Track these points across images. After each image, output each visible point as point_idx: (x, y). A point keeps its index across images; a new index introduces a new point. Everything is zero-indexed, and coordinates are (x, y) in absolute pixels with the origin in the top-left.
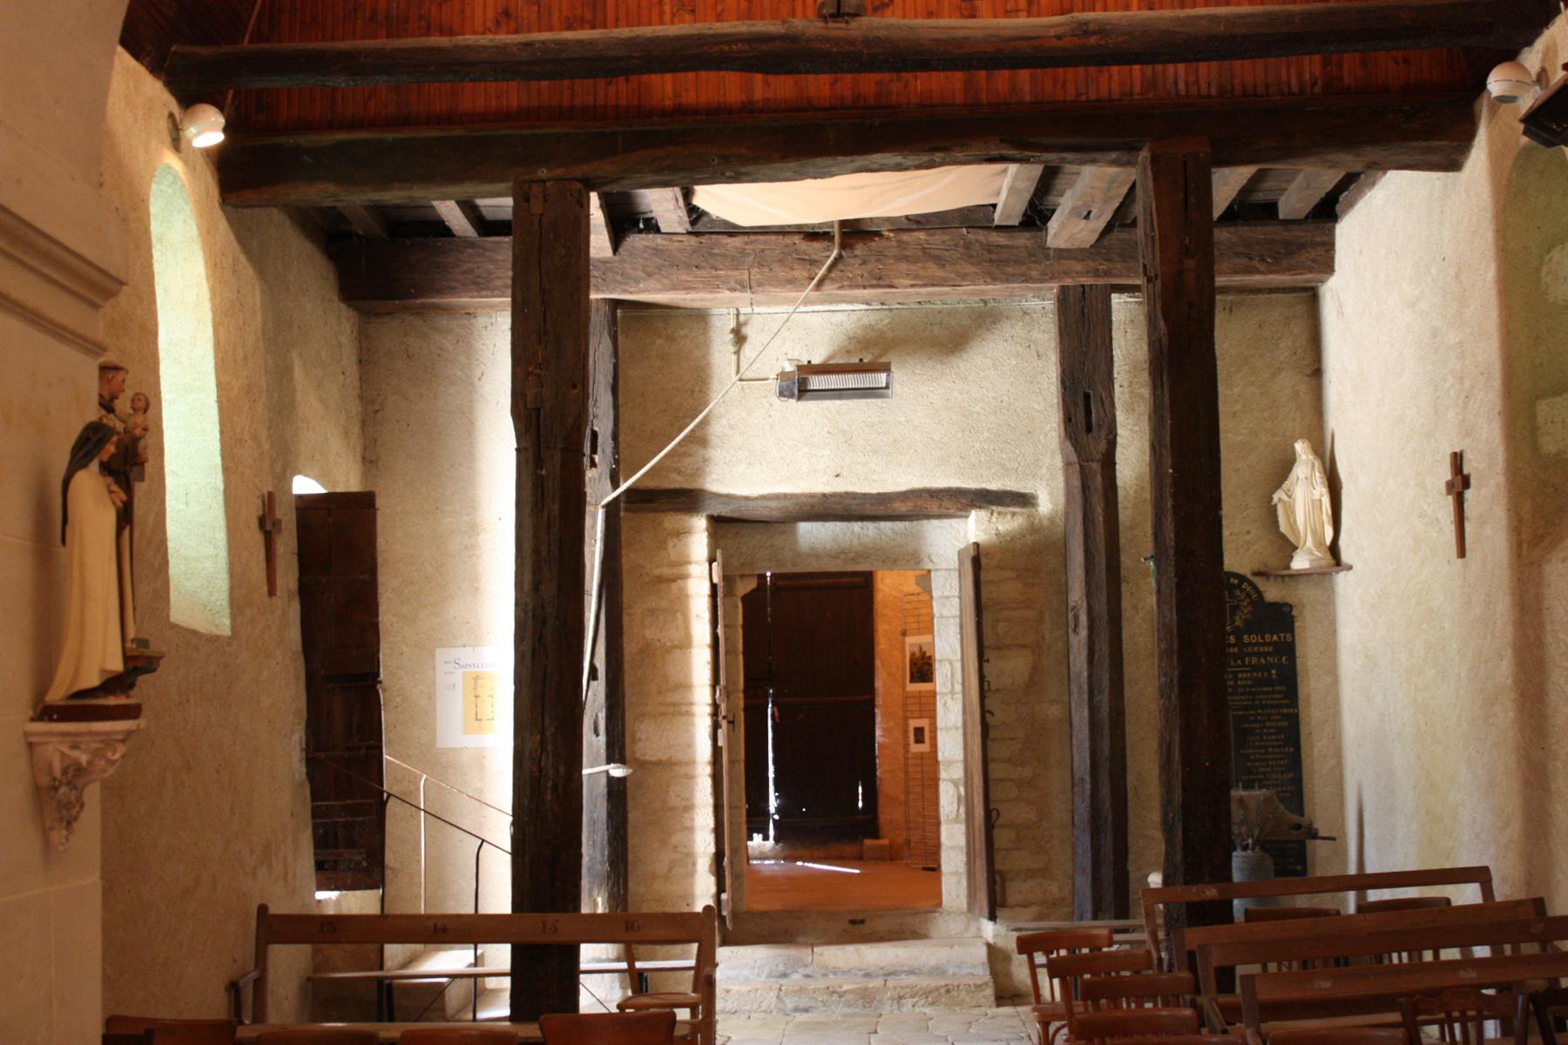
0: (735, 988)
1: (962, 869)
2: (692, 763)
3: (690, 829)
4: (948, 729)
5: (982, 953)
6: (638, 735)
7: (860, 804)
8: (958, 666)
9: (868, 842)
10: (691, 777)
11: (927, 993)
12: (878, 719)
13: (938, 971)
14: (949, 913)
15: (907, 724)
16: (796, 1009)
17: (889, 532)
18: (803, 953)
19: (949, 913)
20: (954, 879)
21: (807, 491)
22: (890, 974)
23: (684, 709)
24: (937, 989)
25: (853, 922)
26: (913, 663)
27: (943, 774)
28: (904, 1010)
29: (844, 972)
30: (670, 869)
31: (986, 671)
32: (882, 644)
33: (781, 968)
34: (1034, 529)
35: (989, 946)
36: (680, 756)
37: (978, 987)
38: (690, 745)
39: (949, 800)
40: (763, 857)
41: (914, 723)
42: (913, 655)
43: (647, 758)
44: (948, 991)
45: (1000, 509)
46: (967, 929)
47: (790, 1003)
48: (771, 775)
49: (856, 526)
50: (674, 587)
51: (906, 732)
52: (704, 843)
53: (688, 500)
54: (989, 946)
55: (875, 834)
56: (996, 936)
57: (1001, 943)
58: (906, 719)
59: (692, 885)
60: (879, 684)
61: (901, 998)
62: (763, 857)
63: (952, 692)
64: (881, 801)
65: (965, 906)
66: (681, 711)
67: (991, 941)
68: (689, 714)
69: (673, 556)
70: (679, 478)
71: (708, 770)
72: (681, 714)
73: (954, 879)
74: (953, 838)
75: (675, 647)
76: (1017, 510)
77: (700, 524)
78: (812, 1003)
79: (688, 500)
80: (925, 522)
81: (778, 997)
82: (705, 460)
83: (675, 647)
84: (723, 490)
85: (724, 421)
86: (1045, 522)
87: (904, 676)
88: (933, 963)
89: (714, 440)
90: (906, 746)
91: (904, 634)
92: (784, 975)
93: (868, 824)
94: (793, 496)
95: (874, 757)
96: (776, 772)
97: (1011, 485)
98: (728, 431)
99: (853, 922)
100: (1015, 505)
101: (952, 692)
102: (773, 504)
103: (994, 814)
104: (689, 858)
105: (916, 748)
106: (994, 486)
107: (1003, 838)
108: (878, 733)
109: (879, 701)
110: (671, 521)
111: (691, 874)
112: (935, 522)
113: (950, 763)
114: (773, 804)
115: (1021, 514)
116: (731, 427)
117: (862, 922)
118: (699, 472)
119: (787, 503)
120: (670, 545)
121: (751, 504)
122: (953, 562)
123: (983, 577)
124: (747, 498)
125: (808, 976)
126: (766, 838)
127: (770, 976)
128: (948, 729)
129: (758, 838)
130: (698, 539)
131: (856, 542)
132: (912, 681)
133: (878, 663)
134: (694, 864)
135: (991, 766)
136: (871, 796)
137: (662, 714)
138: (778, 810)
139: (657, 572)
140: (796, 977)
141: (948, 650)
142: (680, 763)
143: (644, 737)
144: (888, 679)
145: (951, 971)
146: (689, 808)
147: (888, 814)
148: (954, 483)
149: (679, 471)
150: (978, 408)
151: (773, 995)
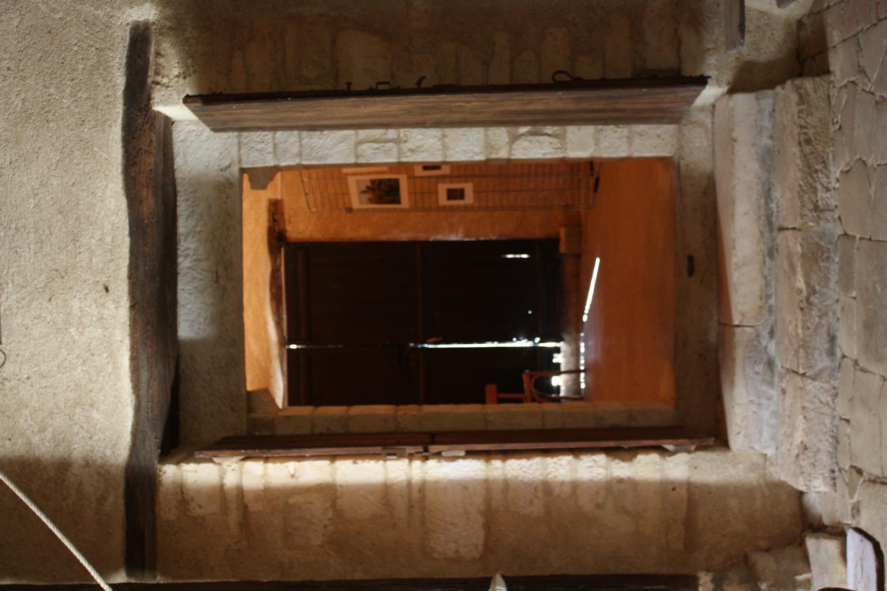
0: (799, 437)
1: (623, 131)
2: (487, 484)
3: (575, 486)
4: (445, 147)
5: (741, 99)
6: (450, 554)
7: (525, 256)
8: (363, 133)
9: (563, 249)
10: (506, 485)
11: (810, 172)
12: (440, 237)
13: (769, 160)
14: (681, 147)
15: (444, 208)
16: (831, 353)
17: (192, 222)
18: (741, 337)
19: (681, 147)
20: (637, 141)
21: (126, 330)
22: (770, 224)
23: (416, 495)
24: (805, 156)
25: (691, 271)
26: (379, 200)
27: (503, 154)
28: (833, 203)
29: (767, 285)
30: (626, 512)
31: (364, 87)
32: (365, 233)
33: (760, 368)
34: (176, 27)
35: (732, 91)
36: (478, 500)
37: (803, 99)
38: (464, 486)
39: (535, 147)
40: (576, 353)
41: (443, 200)
42: (371, 201)
43: (480, 542)
44: (808, 142)
45: (151, 73)
46: (701, 125)
47: (823, 362)
48: (496, 345)
49: (184, 263)
50: (254, 507)
51: (452, 209)
52: (591, 468)
53: (139, 484)
54: (732, 91)
55: (554, 241)
56: (719, 83)
57: (728, 76)
58: (440, 209)
59: (648, 484)
60: (404, 237)
61: (816, 208)
62: (576, 353)
63: (397, 141)
64: (521, 235)
65: (671, 128)
66: (418, 497)
67: (725, 89)
68: (423, 486)
69: (214, 508)
70: (111, 499)
71: (497, 463)
72: (422, 499)
73: (637, 141)
74: (582, 143)
75: (334, 505)
76: (153, 49)
77: (170, 472)
78: (823, 331)
79: (139, 484)
80: (178, 175)
81: (814, 379)
82: (88, 463)
83: (334, 505)
84: (126, 440)
85: (36, 439)
86: (169, 12)
87: (395, 210)
88: (755, 166)
89: (61, 452)
90: (466, 208)
91: (350, 210)
92: (770, 364)
93: (545, 249)
94: (133, 349)
95: (478, 242)
96: (493, 341)
97: (118, 58)
98: (48, 434)
99: (691, 271)
100: (146, 52)
101: (397, 141)
102: (145, 375)
103: (564, 78)
104: (613, 489)
105: (469, 199)
106: (120, 81)
107: (588, 70)
108: (453, 238)
109: (422, 237)
110: (167, 511)
111: (632, 485)
112: (179, 162)
113: (489, 146)
114: (524, 343)
115: (158, 44)
116: (42, 430)
117: (691, 259)
118: (102, 472)
119: (143, 357)
120: (198, 512)
121: (144, 404)
122: (228, 138)
123: (241, 89)
124: (137, 410)
125: (772, 333)
126: (557, 350)
127: (771, 384)
128: (445, 147)
129: (558, 359)
130: (198, 474)
131: (204, 264)
132: (397, 201)
133: (384, 238)
134: (621, 481)
135: (494, 80)
136: (517, 245)
137: (423, 523)
138: (531, 338)
139: (234, 529)
140: (772, 348)
141: (342, 146)
142: (488, 500)
143: (452, 546)
144: (399, 226)
145: (766, 141)
146: (546, 488)
147: (535, 230)
148: (116, 132)
149: (102, 499)
150: (18, 101)
151: (812, 386)
